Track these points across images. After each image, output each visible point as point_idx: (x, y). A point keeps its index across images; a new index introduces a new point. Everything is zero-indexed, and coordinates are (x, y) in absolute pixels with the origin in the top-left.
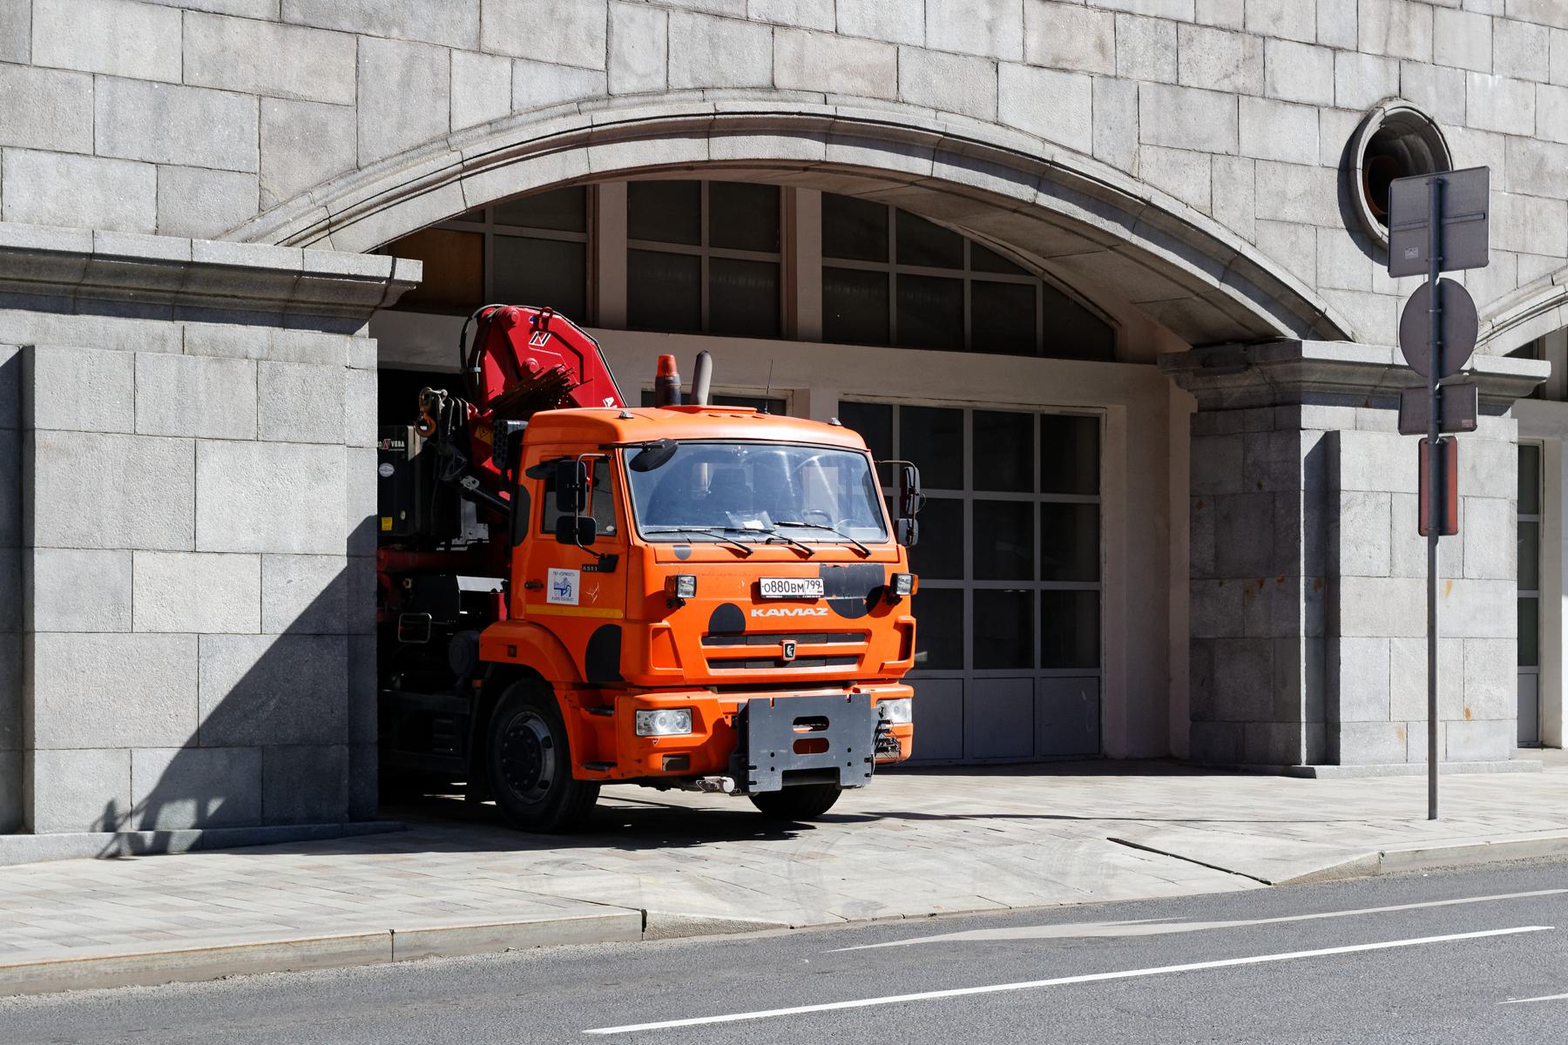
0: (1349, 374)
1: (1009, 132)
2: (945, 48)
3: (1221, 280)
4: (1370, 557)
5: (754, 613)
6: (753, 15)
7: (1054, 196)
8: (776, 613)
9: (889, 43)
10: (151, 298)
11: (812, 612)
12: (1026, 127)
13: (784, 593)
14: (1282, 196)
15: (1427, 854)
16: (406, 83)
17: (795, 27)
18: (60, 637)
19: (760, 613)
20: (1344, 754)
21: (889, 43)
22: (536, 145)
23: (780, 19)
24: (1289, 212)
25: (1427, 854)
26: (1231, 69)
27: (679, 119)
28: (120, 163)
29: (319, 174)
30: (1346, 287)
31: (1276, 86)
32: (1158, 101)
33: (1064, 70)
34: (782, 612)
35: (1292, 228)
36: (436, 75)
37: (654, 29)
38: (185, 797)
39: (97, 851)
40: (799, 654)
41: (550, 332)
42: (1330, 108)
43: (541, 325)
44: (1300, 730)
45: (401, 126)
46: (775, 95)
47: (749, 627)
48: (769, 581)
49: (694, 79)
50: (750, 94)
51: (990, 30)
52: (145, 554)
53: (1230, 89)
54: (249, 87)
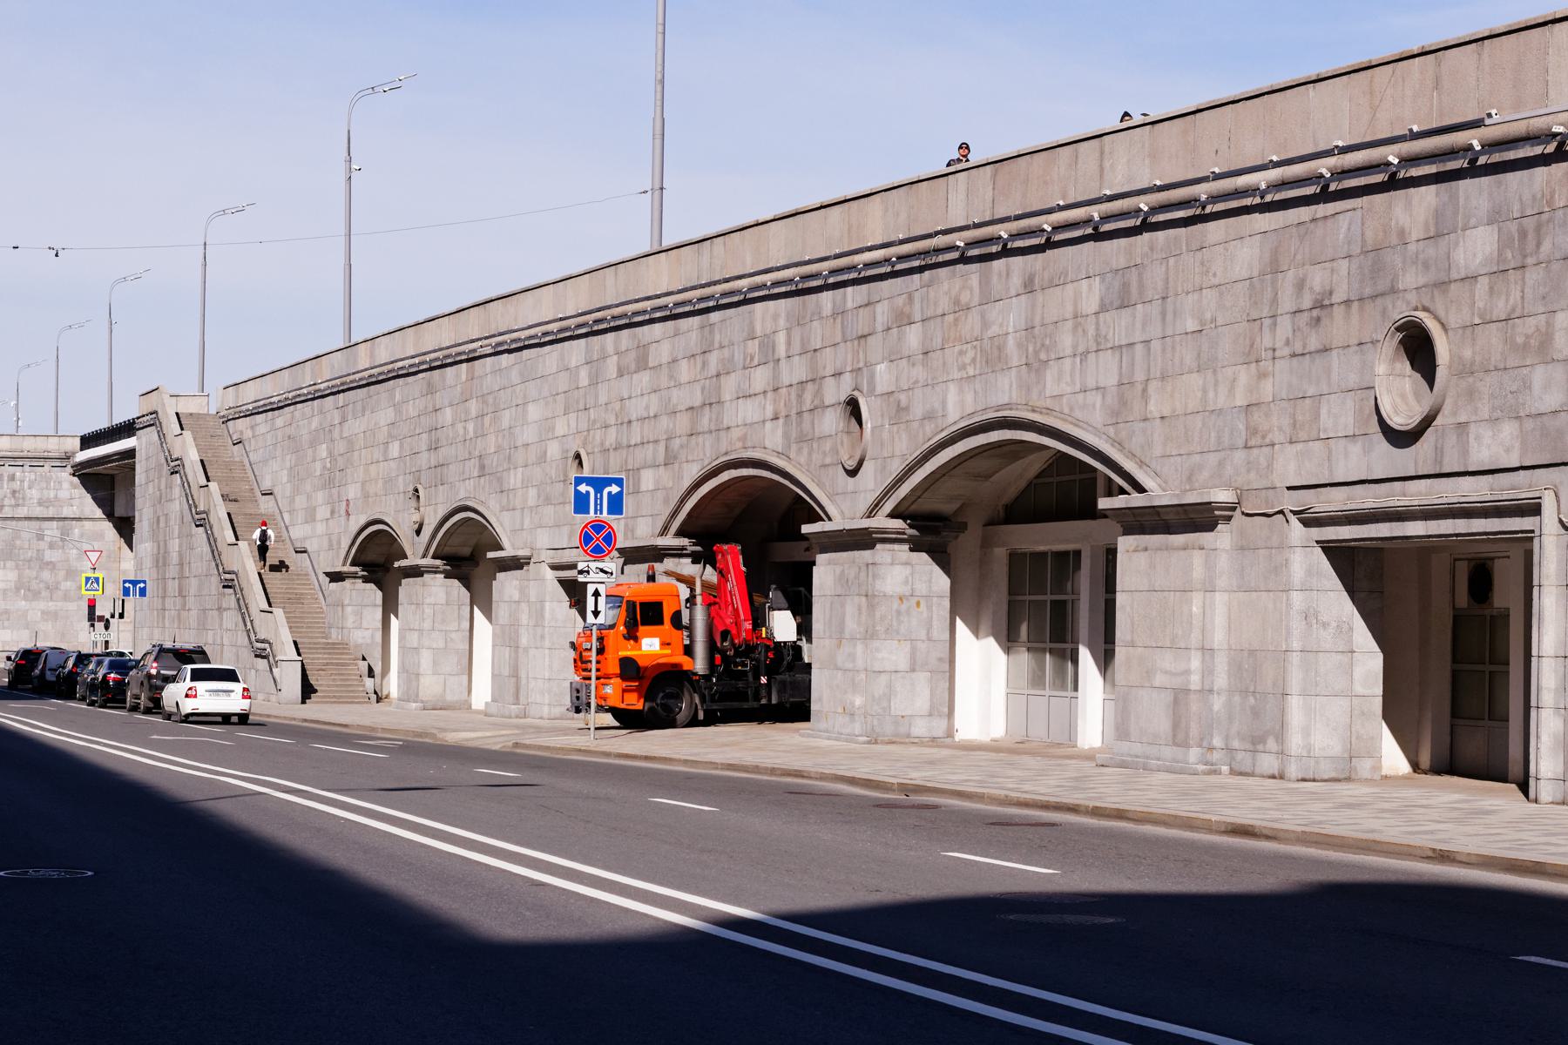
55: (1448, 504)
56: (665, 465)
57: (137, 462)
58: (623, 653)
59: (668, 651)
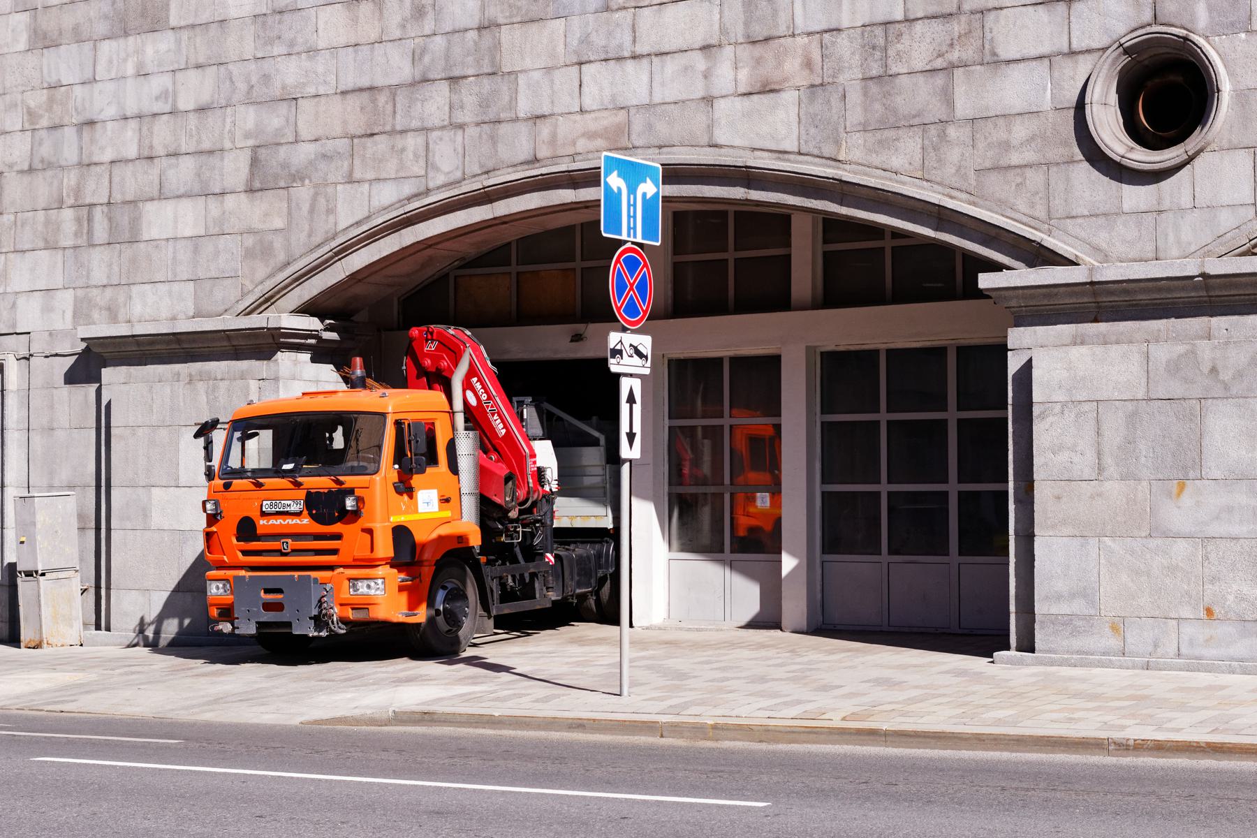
0: (1049, 296)
1: (723, 150)
2: (667, 100)
3: (936, 229)
4: (1071, 462)
5: (261, 522)
6: (521, 115)
7: (763, 190)
8: (275, 522)
9: (622, 108)
10: (176, 353)
11: (298, 522)
12: (737, 142)
13: (278, 510)
14: (1006, 146)
15: (436, 717)
16: (312, 210)
17: (550, 115)
18: (121, 532)
19: (265, 522)
20: (1038, 644)
21: (622, 108)
22: (374, 232)
23: (539, 112)
24: (1015, 158)
25: (436, 717)
26: (944, 48)
27: (461, 196)
28: (178, 283)
29: (269, 270)
30: (1088, 213)
31: (996, 50)
32: (865, 94)
33: (772, 91)
34: (278, 521)
35: (1018, 170)
36: (328, 201)
37: (455, 142)
38: (173, 616)
39: (128, 643)
40: (293, 548)
41: (436, 340)
42: (1064, 54)
43: (431, 337)
44: (1009, 619)
45: (310, 236)
46: (537, 165)
47: (259, 531)
48: (269, 502)
49: (481, 166)
50: (519, 168)
51: (706, 77)
52: (157, 488)
53: (945, 65)
54: (236, 230)
55: (405, 213)
56: (250, 190)
57: (731, 353)
58: (396, 519)
59: (447, 514)
